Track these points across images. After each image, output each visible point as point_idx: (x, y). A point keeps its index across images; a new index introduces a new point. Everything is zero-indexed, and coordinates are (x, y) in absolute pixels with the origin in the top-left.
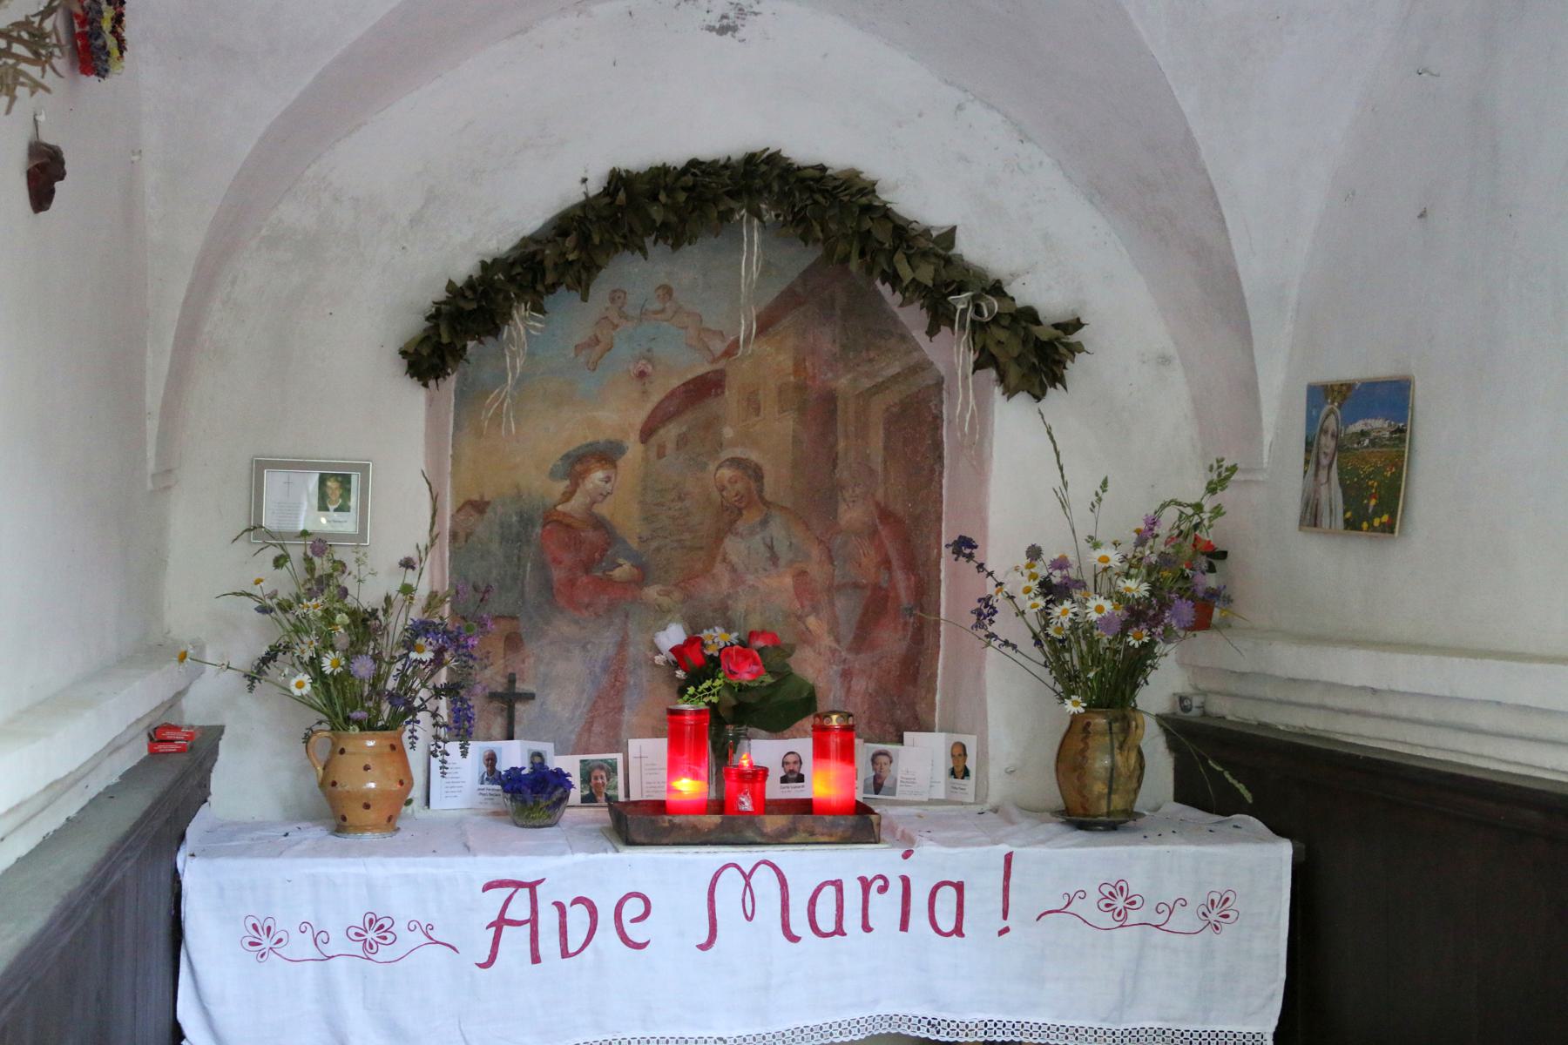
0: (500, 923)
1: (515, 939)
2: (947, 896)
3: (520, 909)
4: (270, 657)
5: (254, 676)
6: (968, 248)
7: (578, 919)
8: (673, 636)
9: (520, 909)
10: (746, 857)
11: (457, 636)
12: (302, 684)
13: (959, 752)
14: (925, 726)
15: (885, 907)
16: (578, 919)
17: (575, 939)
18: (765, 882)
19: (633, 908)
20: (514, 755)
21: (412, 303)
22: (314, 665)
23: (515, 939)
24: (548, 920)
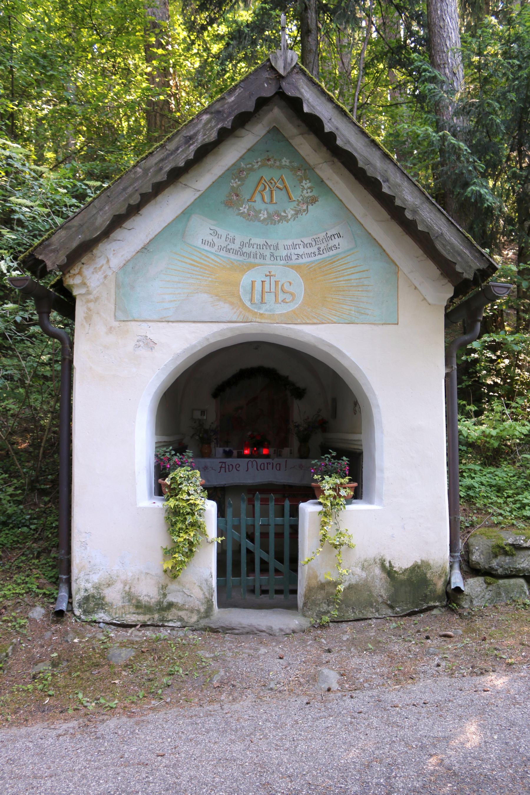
0: (221, 467)
1: (223, 469)
2: (278, 466)
3: (223, 466)
4: (194, 435)
5: (192, 437)
6: (291, 379)
7: (231, 467)
8: (249, 433)
9: (223, 466)
10: (252, 460)
11: (35, 372)
12: (197, 438)
13: (291, 450)
14: (287, 446)
15: (270, 467)
16: (231, 467)
17: (231, 469)
18: (254, 463)
19: (238, 466)
20: (227, 449)
21: (123, 598)
22: (199, 436)
23: (223, 469)
24: (227, 467)
